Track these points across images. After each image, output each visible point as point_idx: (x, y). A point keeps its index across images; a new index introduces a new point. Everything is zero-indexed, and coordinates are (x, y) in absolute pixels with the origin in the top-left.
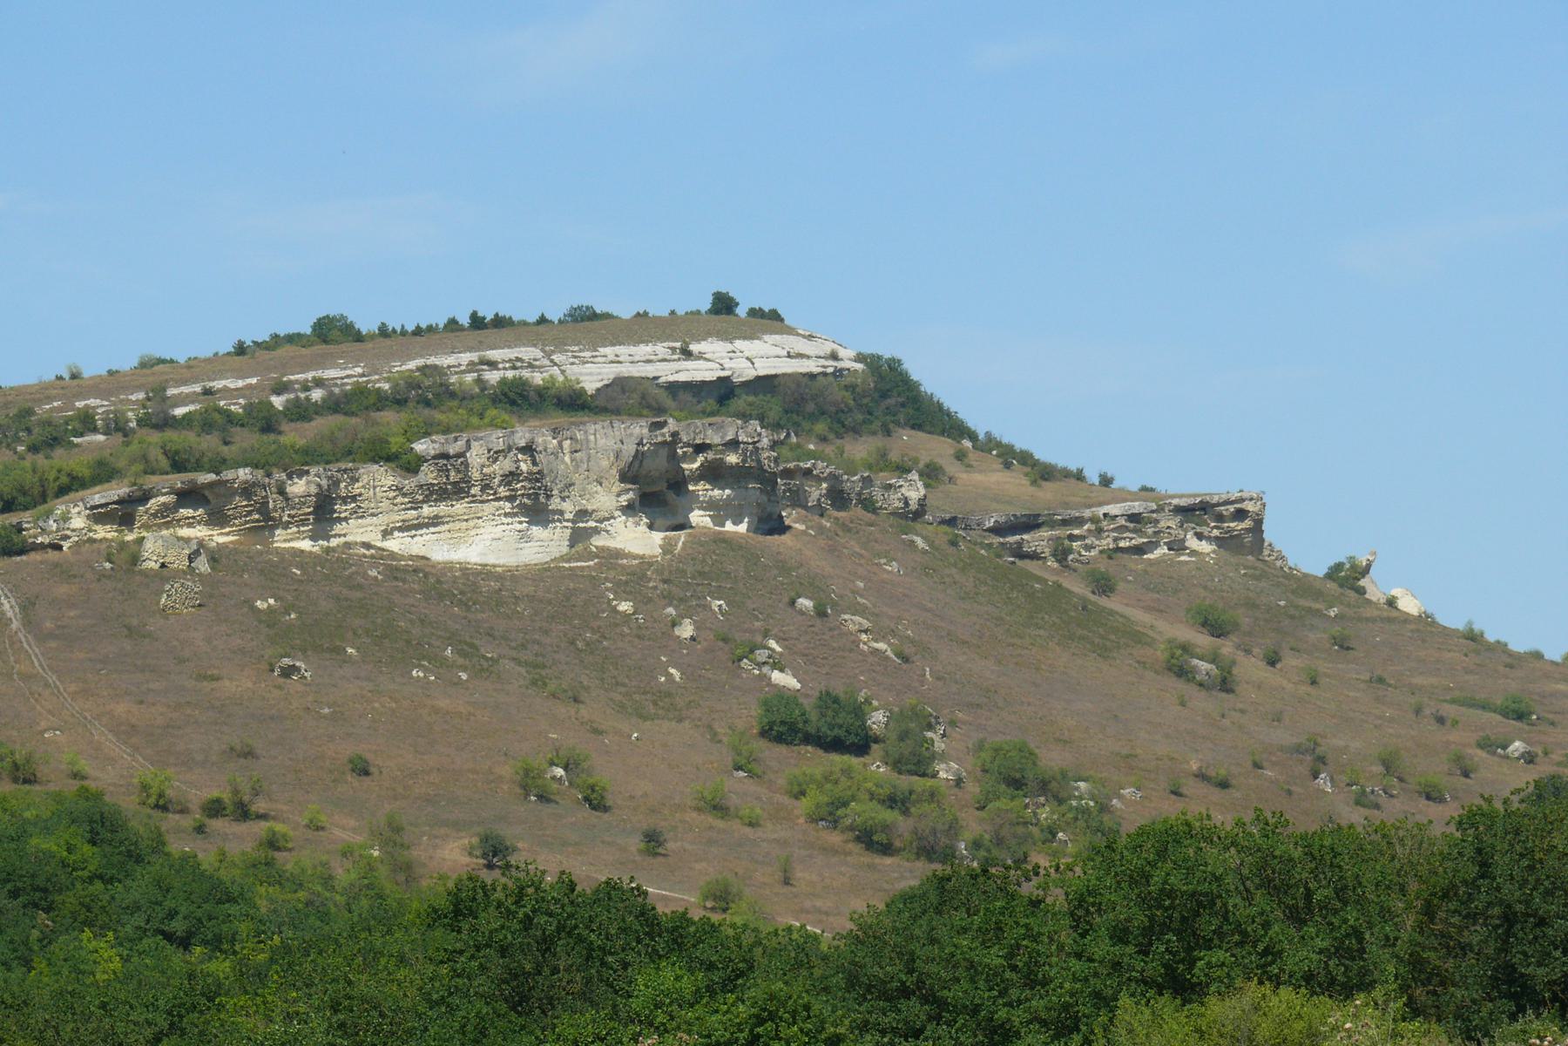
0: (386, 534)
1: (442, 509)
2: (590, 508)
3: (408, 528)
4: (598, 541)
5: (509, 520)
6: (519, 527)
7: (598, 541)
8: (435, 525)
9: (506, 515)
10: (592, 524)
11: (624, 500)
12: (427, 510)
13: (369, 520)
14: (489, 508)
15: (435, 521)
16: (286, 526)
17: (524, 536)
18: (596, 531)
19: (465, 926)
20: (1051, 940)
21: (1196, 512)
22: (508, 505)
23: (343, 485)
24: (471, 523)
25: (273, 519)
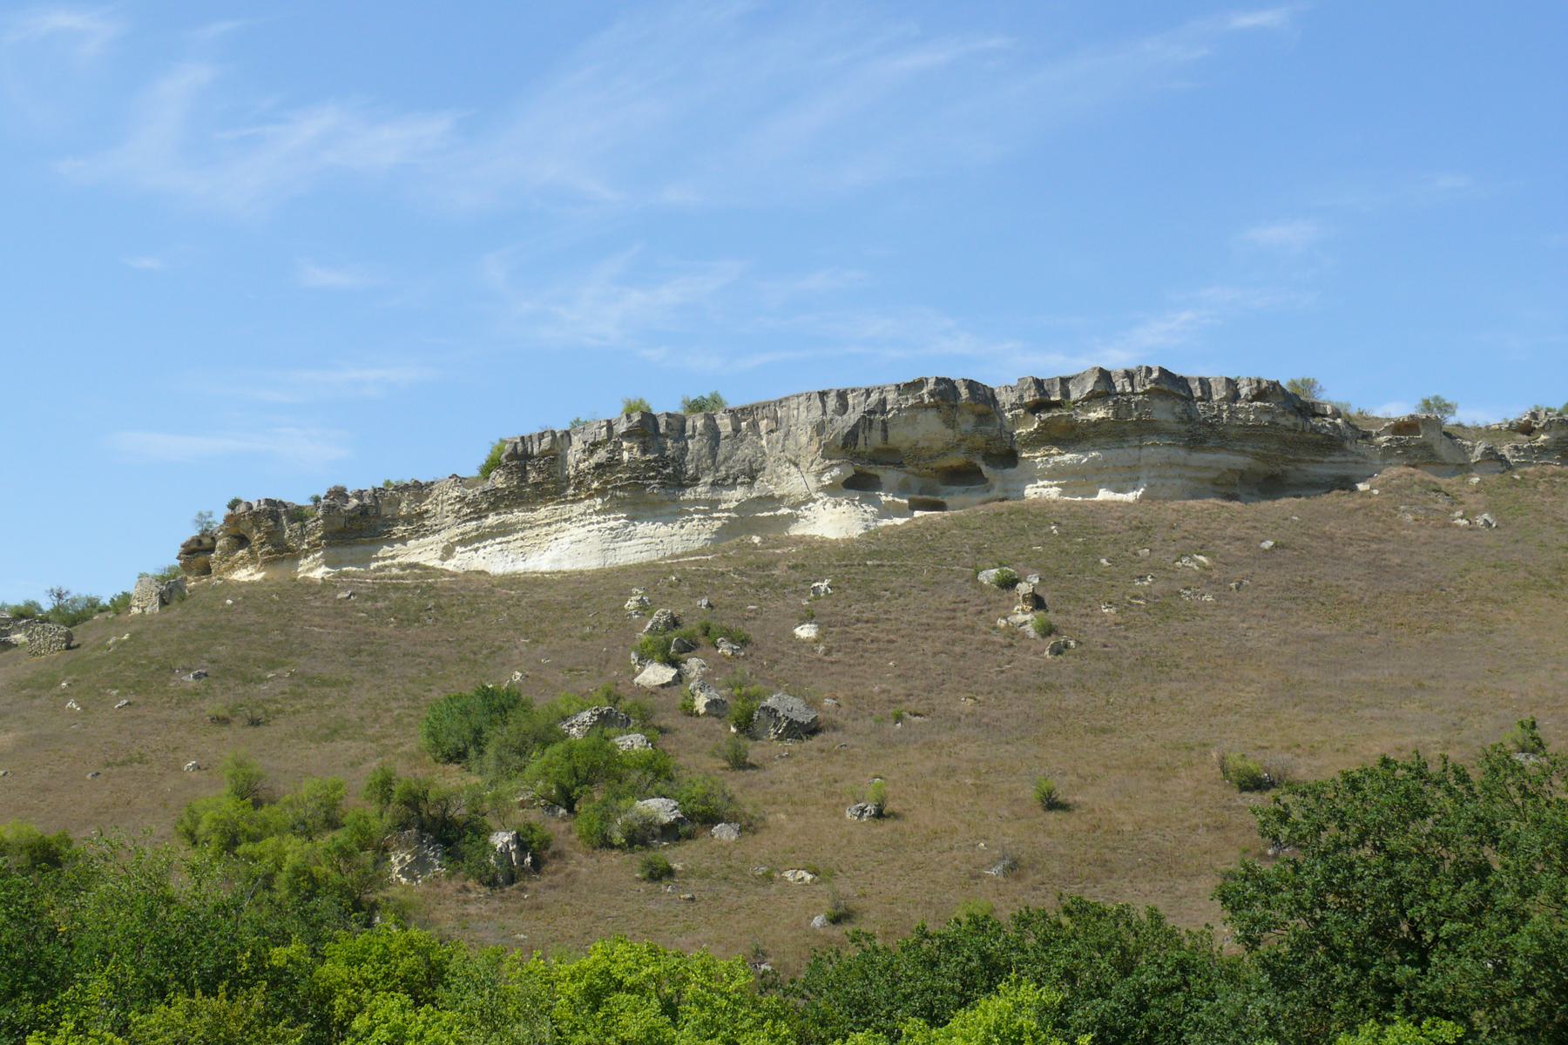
0: (448, 552)
1: (518, 515)
2: (777, 493)
3: (471, 541)
4: (796, 531)
5: (601, 518)
6: (612, 524)
7: (796, 531)
8: (504, 534)
9: (597, 513)
10: (784, 511)
11: (826, 479)
12: (492, 519)
13: (431, 539)
14: (578, 508)
15: (504, 530)
16: (306, 554)
17: (616, 535)
18: (793, 519)
19: (208, 1019)
20: (1363, 1005)
21: (197, 552)
22: (599, 500)
23: (403, 505)
24: (554, 527)
25: (289, 549)
